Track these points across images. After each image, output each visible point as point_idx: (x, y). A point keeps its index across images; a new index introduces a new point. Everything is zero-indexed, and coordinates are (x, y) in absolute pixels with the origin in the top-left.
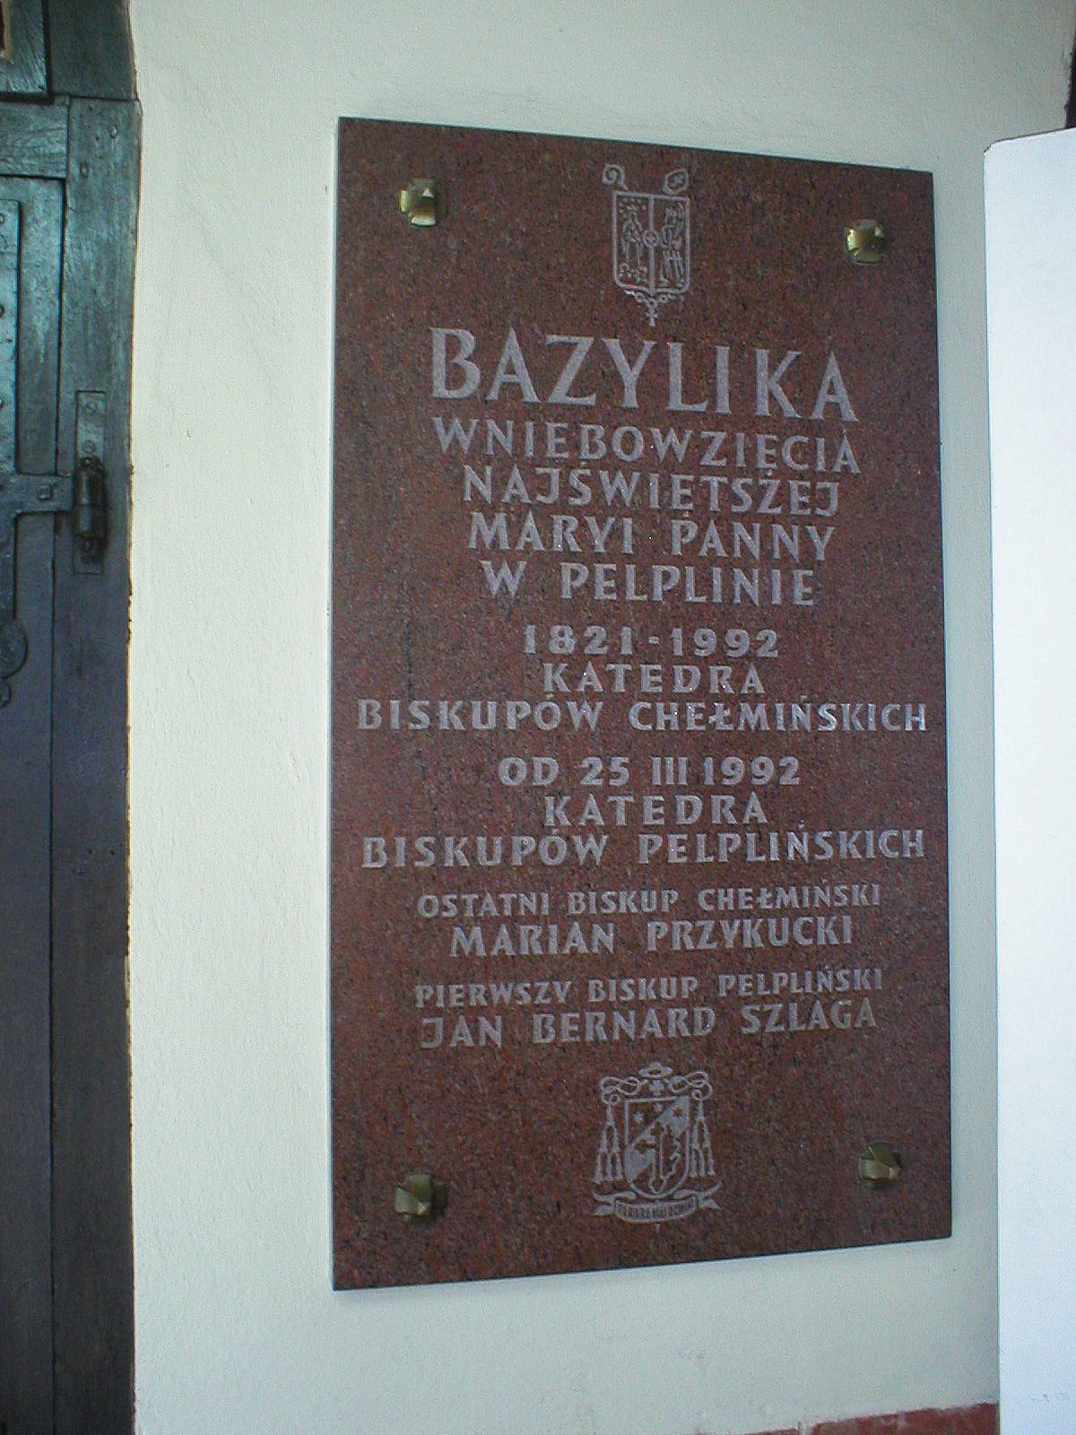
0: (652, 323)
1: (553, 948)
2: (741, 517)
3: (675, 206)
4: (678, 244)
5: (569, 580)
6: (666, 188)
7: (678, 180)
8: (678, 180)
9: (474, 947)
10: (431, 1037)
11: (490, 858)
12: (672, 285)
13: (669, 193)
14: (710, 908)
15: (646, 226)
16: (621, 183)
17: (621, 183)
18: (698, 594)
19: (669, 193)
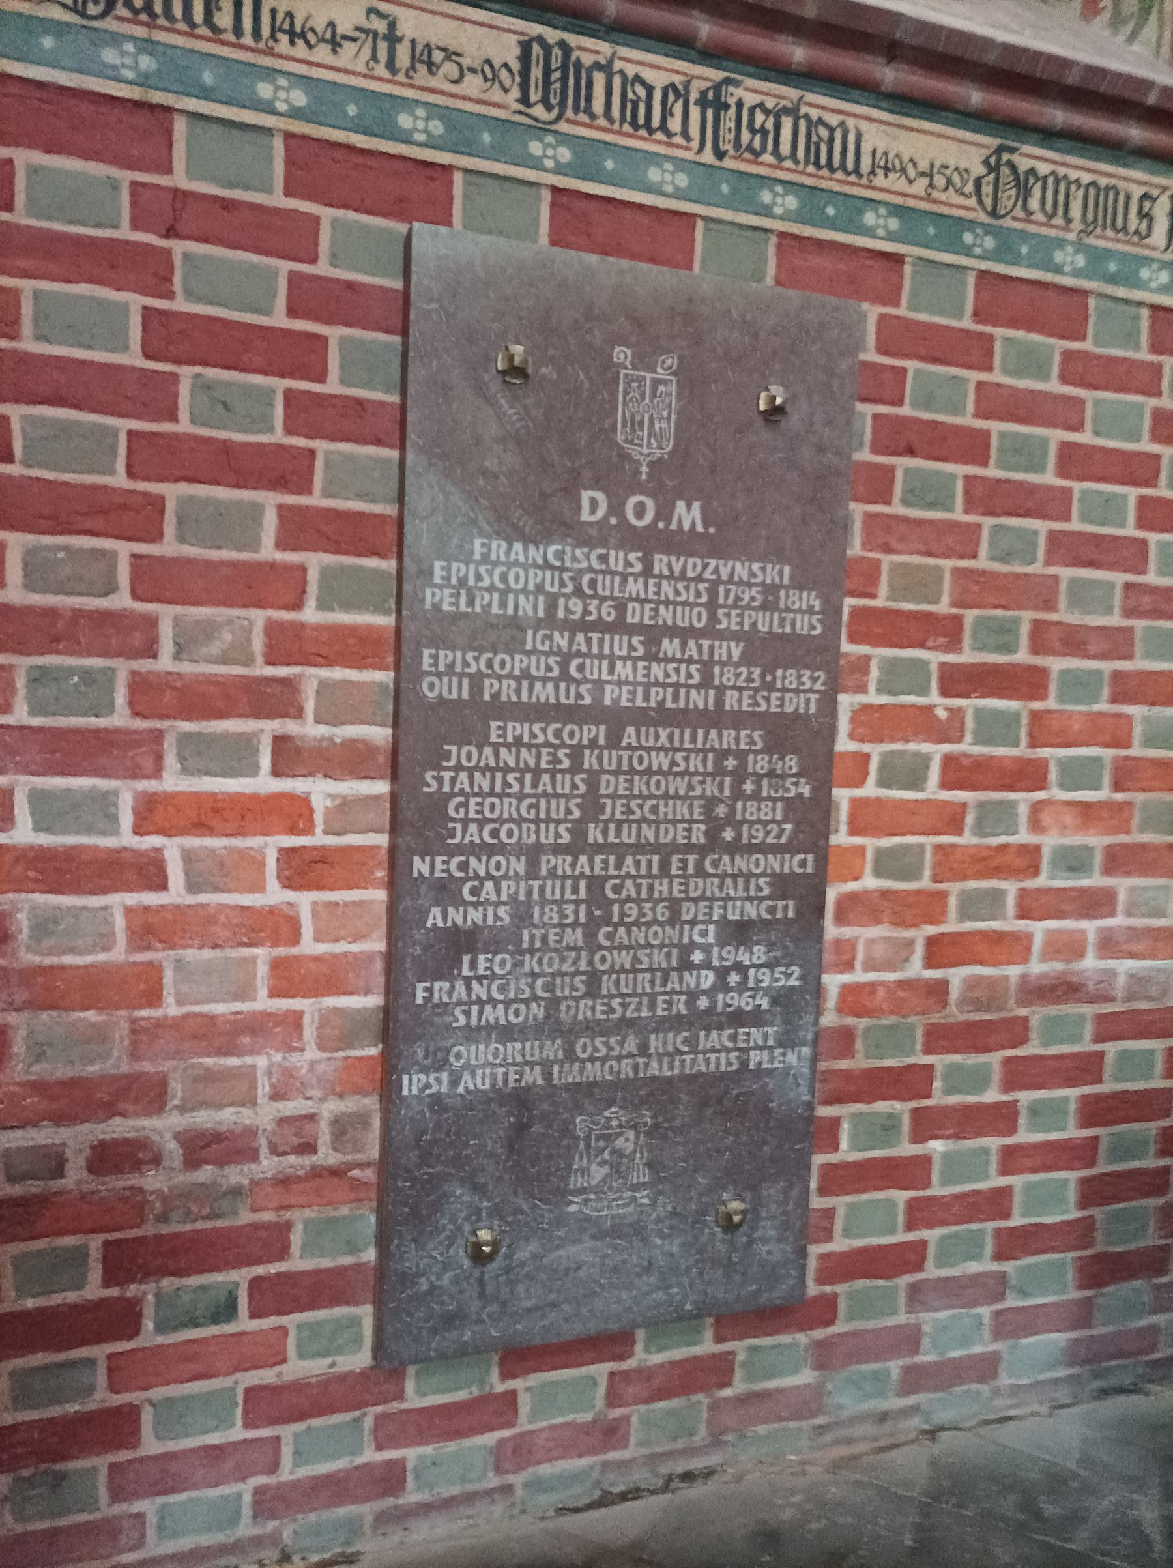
0: (644, 477)
1: (524, 698)
2: (512, 770)
3: (664, 382)
4: (665, 414)
5: (520, 866)
6: (659, 370)
7: (669, 362)
8: (669, 362)
9: (693, 524)
10: (453, 837)
11: (568, 698)
12: (660, 447)
13: (661, 373)
14: (608, 943)
15: (643, 398)
16: (628, 364)
17: (628, 364)
18: (148, 763)
19: (661, 373)
